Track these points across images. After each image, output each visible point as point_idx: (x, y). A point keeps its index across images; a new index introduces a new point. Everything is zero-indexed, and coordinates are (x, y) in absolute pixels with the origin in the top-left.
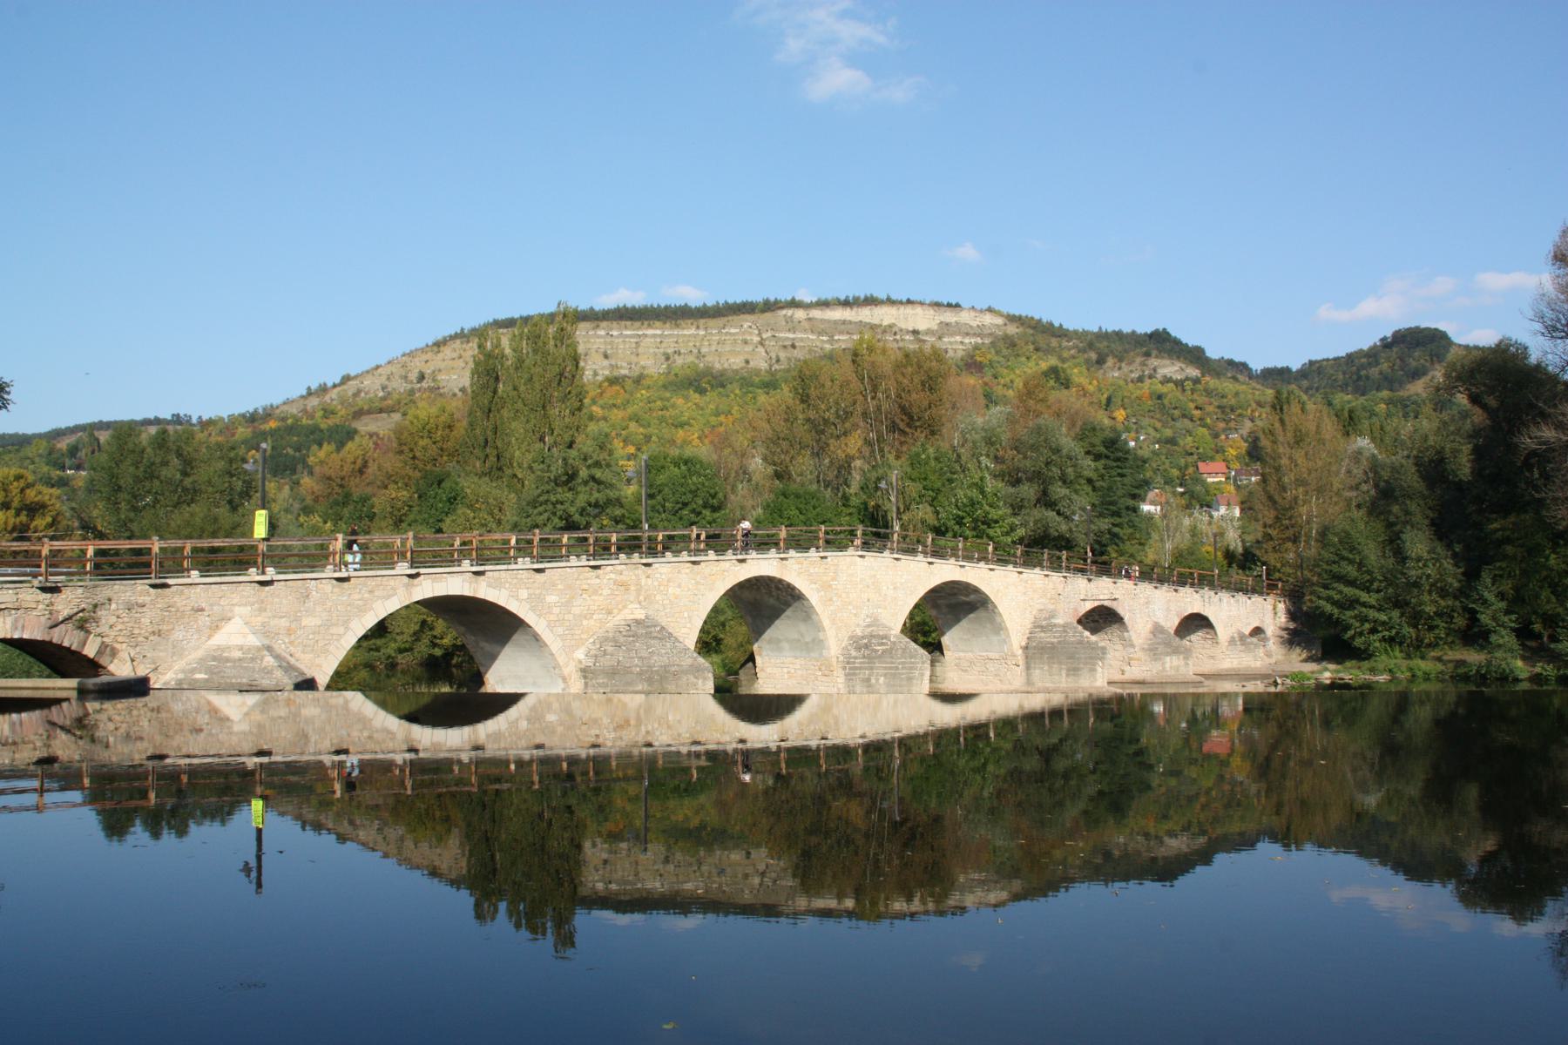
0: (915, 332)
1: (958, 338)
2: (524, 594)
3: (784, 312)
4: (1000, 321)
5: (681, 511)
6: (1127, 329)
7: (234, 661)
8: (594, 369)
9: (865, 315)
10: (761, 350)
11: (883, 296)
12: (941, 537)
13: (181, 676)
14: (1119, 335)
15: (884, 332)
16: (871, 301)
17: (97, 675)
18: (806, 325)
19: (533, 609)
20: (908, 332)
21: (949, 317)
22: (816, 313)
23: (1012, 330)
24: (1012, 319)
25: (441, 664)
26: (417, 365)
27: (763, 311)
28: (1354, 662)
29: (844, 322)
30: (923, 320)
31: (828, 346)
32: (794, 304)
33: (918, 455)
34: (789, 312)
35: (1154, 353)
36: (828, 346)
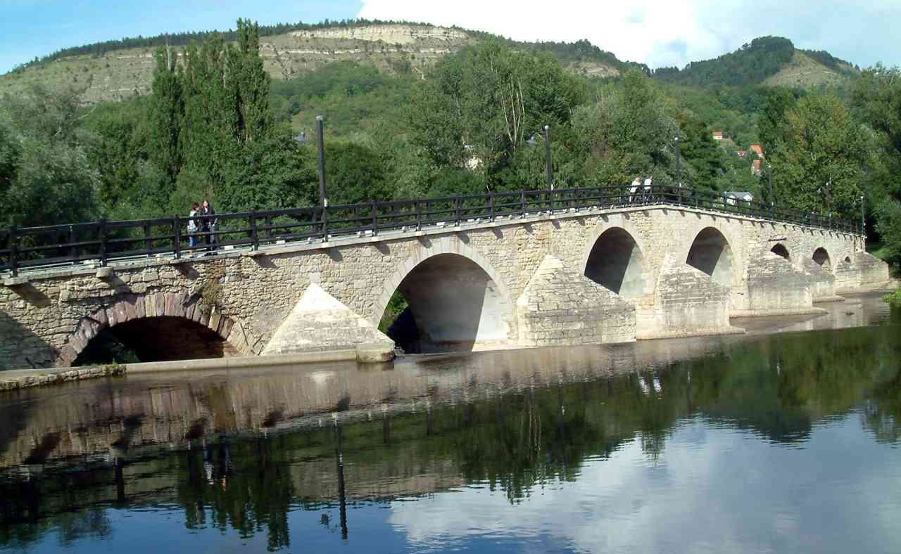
0: (398, 46)
1: (432, 50)
2: (486, 250)
3: (294, 34)
4: (462, 35)
5: (345, 200)
6: (558, 40)
7: (329, 325)
8: (275, 72)
9: (358, 33)
10: (277, 64)
11: (371, 19)
12: (581, 195)
13: (284, 343)
14: (552, 46)
15: (374, 46)
16: (363, 23)
17: (220, 355)
18: (311, 43)
19: (492, 263)
20: (392, 46)
21: (421, 33)
22: (318, 34)
23: (473, 42)
24: (472, 34)
25: (423, 317)
26: (56, 82)
27: (279, 34)
28: (417, 320)
29: (342, 40)
30: (403, 37)
31: (330, 60)
32: (301, 27)
33: (137, 196)
34: (298, 34)
35: (584, 57)
36: (330, 60)
